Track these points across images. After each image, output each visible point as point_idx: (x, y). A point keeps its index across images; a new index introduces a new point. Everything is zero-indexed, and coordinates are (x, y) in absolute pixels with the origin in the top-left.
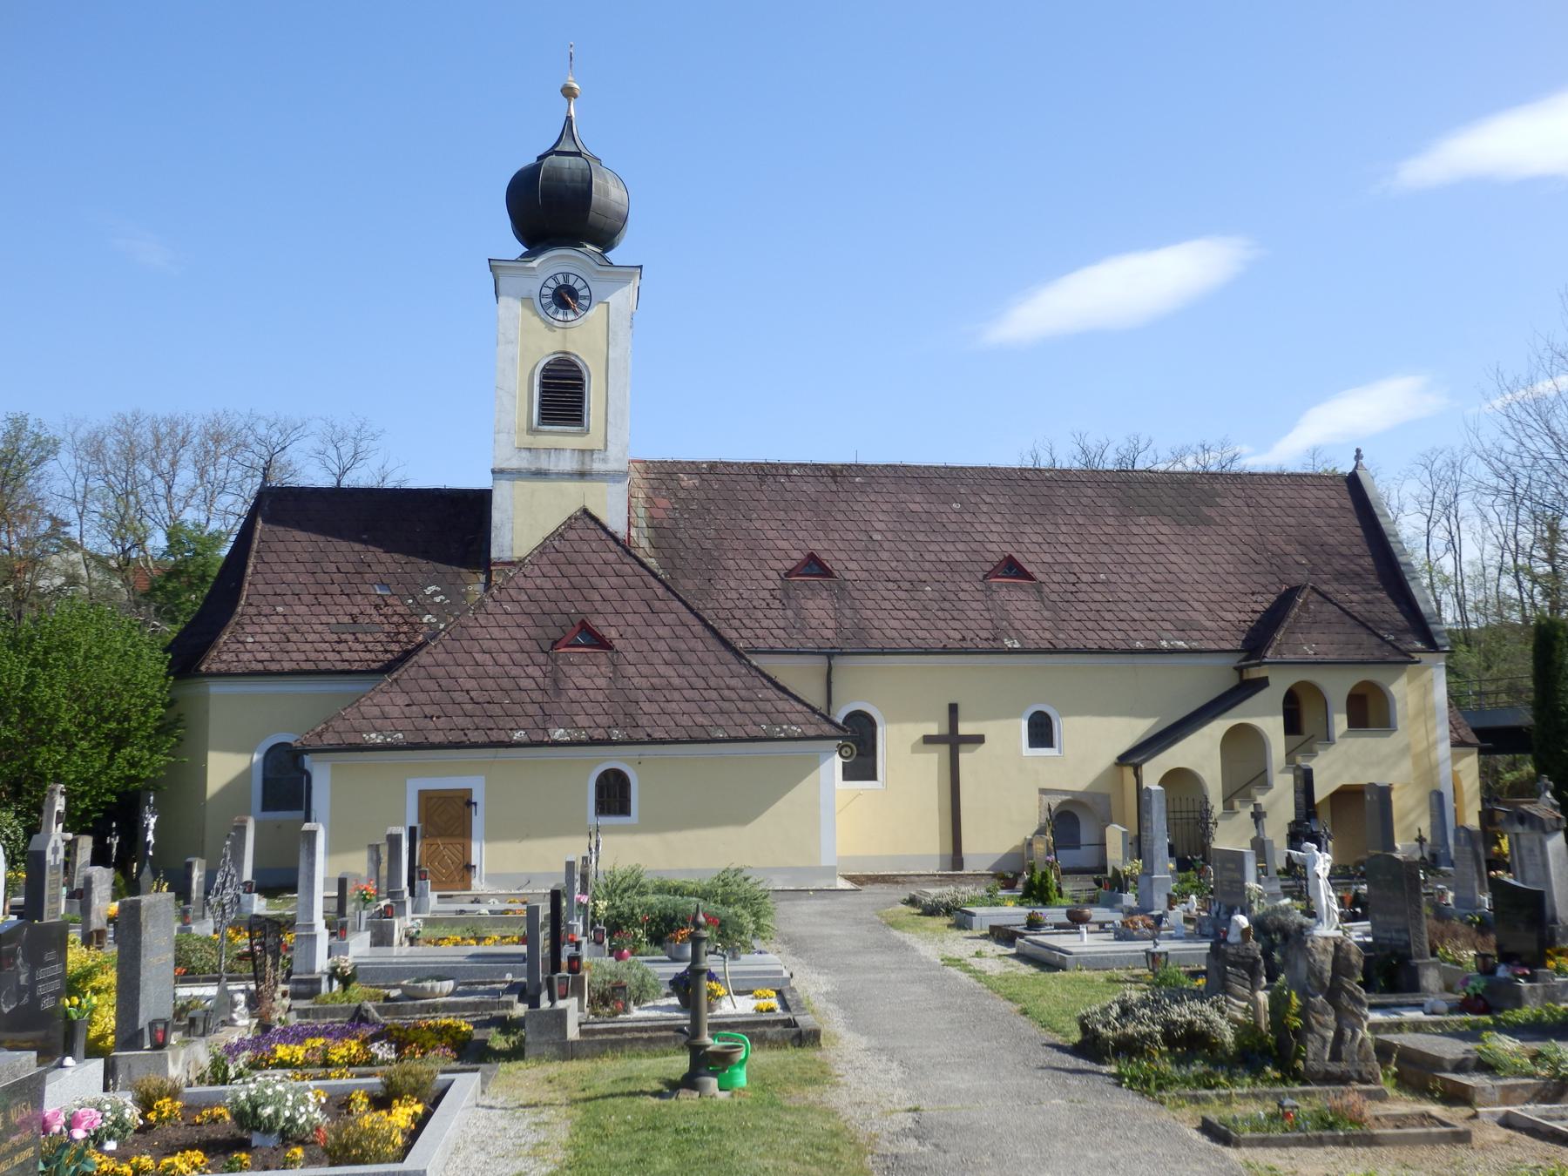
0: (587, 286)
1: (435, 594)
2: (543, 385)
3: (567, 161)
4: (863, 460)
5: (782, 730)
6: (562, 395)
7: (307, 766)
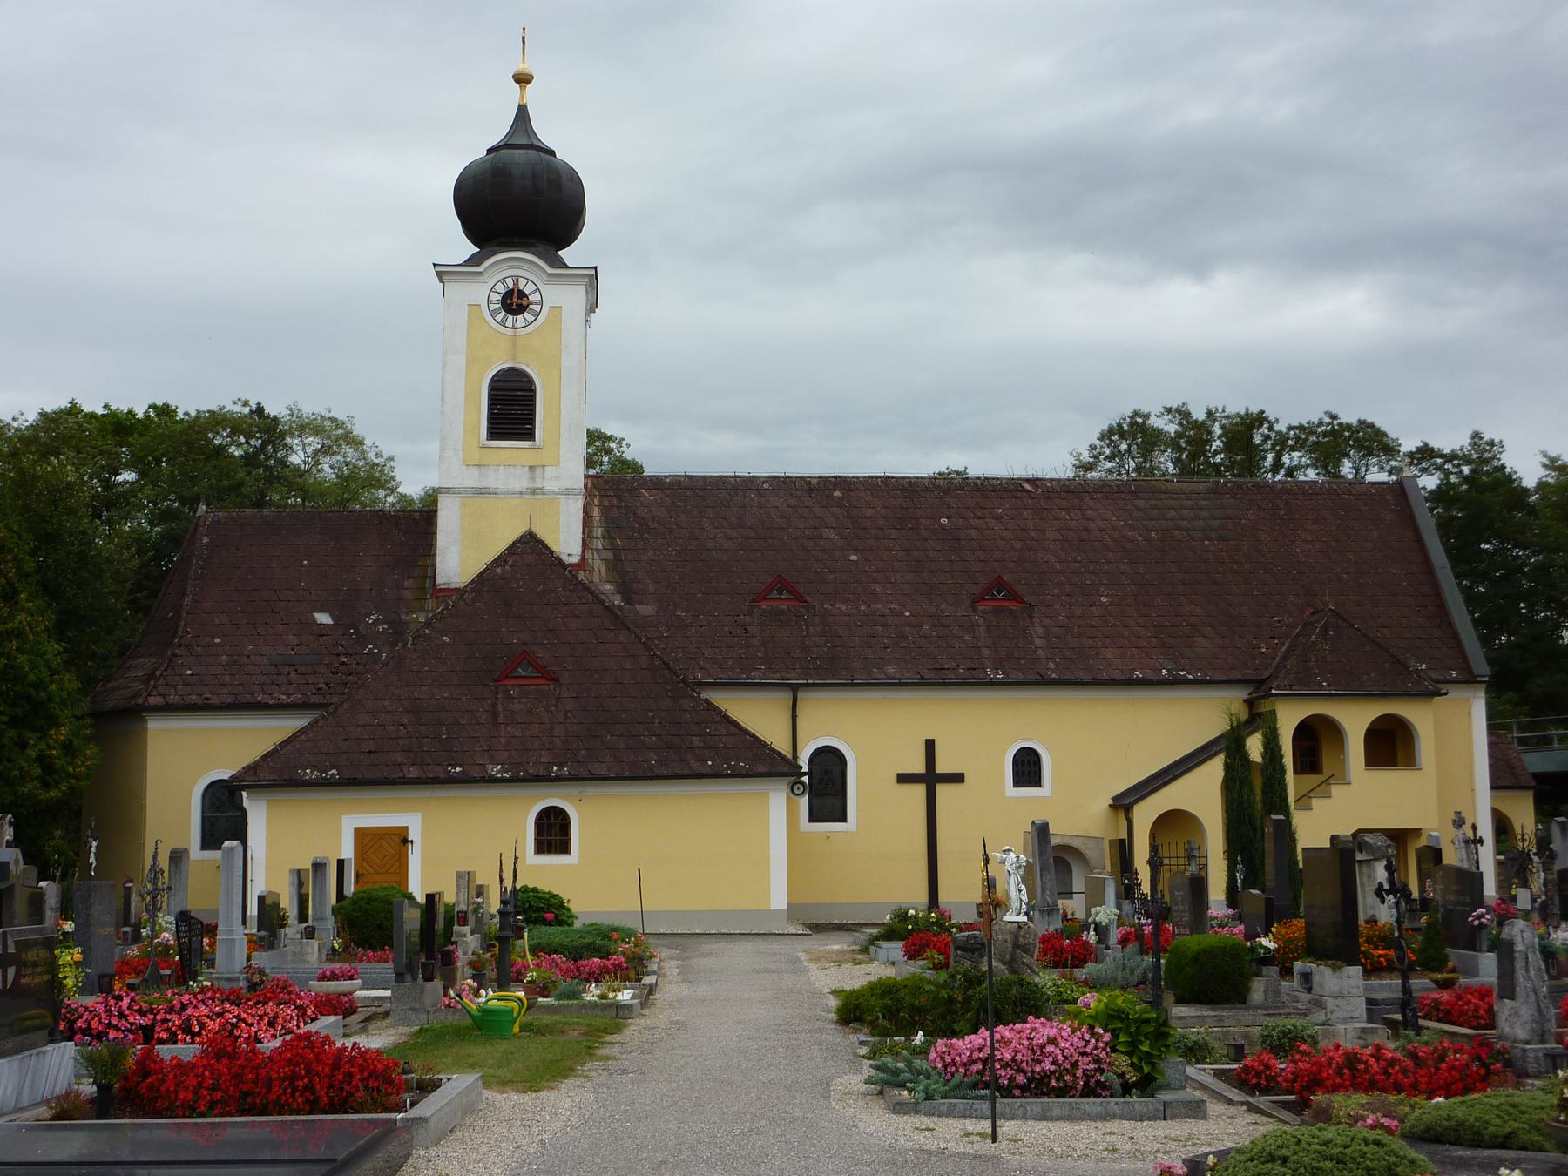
0: (538, 289)
1: (377, 623)
2: (491, 397)
3: (519, 154)
4: (841, 472)
5: (730, 767)
6: (512, 408)
7: (246, 803)
